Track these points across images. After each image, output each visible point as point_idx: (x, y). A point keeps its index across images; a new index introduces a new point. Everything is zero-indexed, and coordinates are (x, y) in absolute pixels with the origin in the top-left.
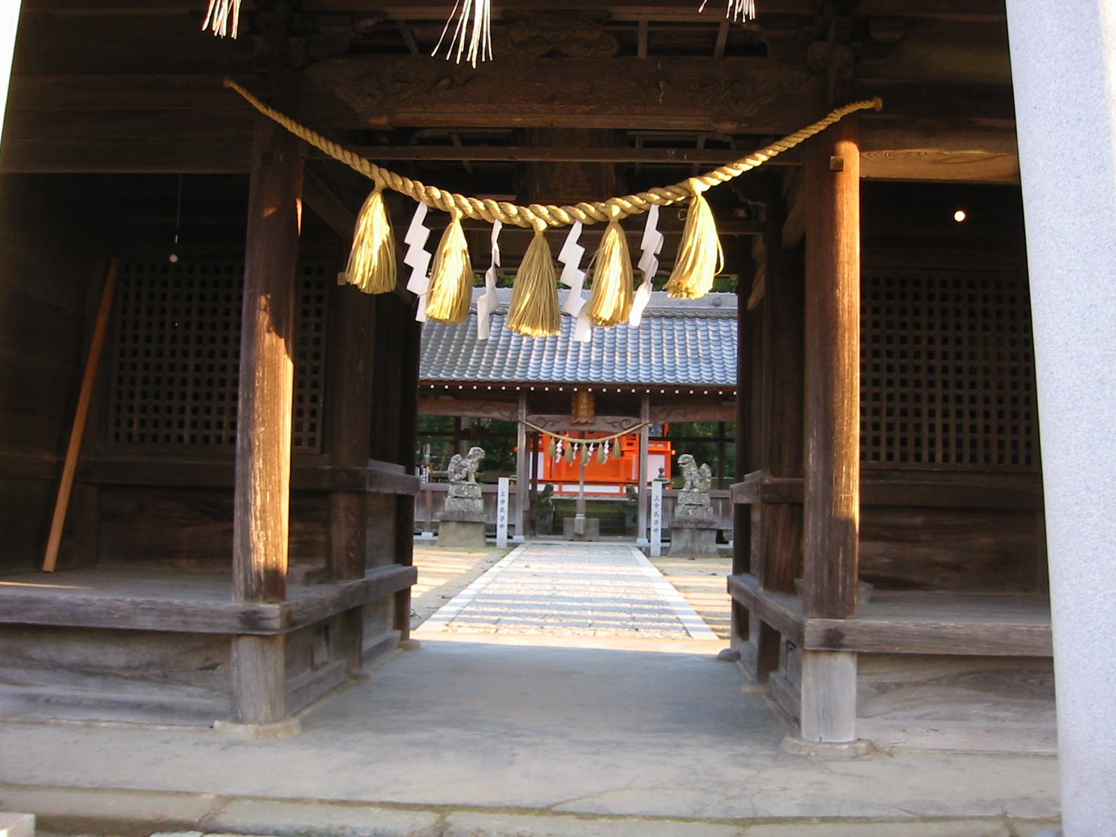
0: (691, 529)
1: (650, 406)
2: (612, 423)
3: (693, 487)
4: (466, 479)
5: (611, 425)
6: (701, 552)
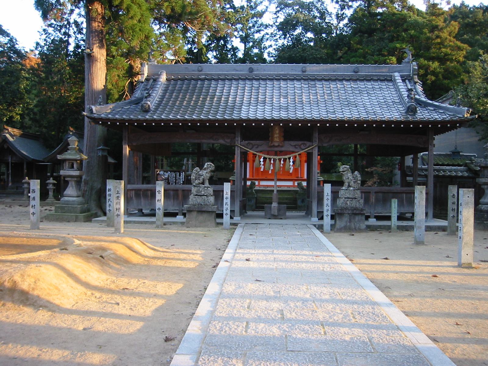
0: (349, 214)
1: (318, 135)
2: (295, 146)
3: (349, 186)
4: (203, 183)
5: (294, 147)
6: (355, 229)
